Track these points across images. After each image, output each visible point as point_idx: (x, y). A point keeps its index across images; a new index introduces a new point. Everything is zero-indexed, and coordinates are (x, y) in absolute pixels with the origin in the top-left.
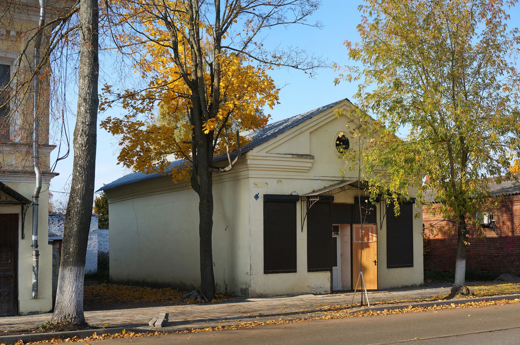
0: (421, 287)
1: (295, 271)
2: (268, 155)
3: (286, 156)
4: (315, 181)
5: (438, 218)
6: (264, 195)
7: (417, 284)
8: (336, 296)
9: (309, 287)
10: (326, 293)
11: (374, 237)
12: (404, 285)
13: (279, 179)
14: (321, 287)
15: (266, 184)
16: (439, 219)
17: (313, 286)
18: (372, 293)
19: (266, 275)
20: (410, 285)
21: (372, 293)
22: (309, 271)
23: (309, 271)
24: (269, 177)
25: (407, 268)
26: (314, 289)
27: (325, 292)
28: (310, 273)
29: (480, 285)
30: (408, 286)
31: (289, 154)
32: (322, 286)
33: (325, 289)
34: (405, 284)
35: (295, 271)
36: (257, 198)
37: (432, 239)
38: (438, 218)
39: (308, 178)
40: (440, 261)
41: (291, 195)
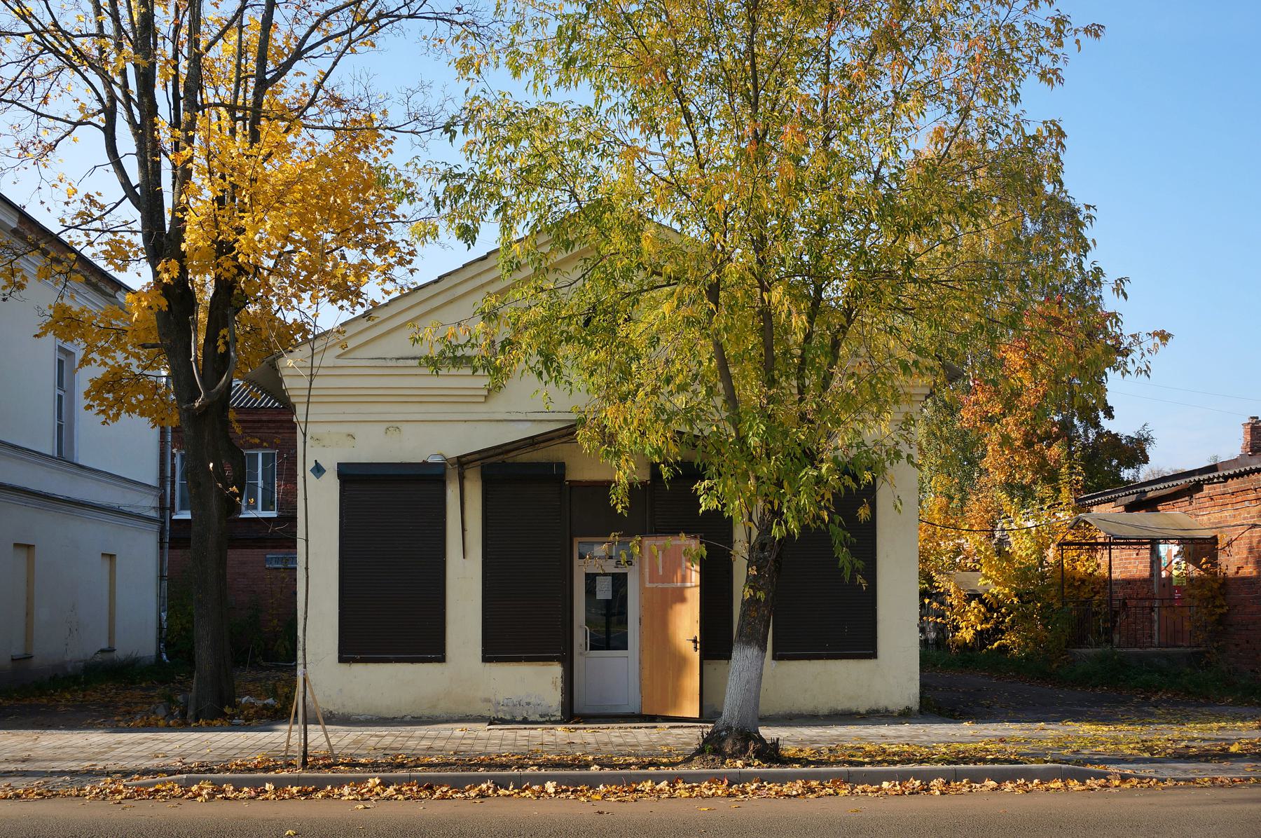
0: (905, 716)
1: (441, 659)
2: (340, 362)
3: (401, 363)
4: (512, 424)
5: (1245, 519)
6: (339, 464)
7: (891, 708)
8: (536, 729)
9: (488, 700)
10: (546, 720)
11: (693, 573)
12: (839, 708)
13: (391, 424)
14: (528, 704)
15: (350, 438)
16: (1245, 522)
17: (501, 699)
18: (671, 727)
19: (345, 666)
20: (862, 710)
21: (671, 727)
22: (486, 659)
23: (486, 659)
24: (332, 418)
25: (844, 661)
26: (505, 708)
27: (541, 716)
28: (492, 665)
29: (1183, 720)
30: (858, 713)
31: (412, 358)
32: (533, 700)
33: (541, 710)
34: (844, 705)
35: (441, 659)
36: (318, 471)
37: (1232, 579)
38: (1245, 519)
39: (485, 417)
40: (1248, 642)
41: (425, 463)
